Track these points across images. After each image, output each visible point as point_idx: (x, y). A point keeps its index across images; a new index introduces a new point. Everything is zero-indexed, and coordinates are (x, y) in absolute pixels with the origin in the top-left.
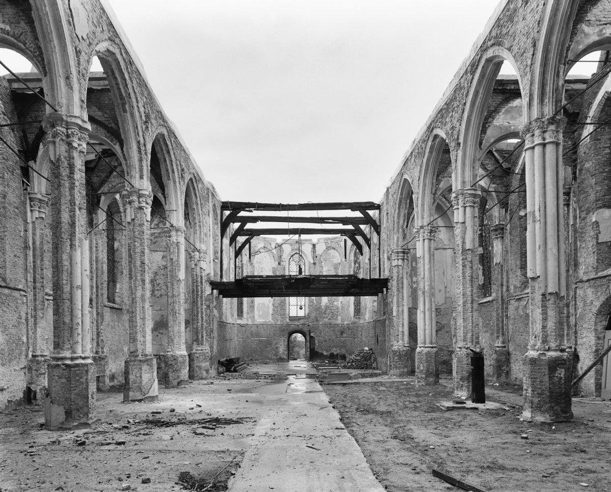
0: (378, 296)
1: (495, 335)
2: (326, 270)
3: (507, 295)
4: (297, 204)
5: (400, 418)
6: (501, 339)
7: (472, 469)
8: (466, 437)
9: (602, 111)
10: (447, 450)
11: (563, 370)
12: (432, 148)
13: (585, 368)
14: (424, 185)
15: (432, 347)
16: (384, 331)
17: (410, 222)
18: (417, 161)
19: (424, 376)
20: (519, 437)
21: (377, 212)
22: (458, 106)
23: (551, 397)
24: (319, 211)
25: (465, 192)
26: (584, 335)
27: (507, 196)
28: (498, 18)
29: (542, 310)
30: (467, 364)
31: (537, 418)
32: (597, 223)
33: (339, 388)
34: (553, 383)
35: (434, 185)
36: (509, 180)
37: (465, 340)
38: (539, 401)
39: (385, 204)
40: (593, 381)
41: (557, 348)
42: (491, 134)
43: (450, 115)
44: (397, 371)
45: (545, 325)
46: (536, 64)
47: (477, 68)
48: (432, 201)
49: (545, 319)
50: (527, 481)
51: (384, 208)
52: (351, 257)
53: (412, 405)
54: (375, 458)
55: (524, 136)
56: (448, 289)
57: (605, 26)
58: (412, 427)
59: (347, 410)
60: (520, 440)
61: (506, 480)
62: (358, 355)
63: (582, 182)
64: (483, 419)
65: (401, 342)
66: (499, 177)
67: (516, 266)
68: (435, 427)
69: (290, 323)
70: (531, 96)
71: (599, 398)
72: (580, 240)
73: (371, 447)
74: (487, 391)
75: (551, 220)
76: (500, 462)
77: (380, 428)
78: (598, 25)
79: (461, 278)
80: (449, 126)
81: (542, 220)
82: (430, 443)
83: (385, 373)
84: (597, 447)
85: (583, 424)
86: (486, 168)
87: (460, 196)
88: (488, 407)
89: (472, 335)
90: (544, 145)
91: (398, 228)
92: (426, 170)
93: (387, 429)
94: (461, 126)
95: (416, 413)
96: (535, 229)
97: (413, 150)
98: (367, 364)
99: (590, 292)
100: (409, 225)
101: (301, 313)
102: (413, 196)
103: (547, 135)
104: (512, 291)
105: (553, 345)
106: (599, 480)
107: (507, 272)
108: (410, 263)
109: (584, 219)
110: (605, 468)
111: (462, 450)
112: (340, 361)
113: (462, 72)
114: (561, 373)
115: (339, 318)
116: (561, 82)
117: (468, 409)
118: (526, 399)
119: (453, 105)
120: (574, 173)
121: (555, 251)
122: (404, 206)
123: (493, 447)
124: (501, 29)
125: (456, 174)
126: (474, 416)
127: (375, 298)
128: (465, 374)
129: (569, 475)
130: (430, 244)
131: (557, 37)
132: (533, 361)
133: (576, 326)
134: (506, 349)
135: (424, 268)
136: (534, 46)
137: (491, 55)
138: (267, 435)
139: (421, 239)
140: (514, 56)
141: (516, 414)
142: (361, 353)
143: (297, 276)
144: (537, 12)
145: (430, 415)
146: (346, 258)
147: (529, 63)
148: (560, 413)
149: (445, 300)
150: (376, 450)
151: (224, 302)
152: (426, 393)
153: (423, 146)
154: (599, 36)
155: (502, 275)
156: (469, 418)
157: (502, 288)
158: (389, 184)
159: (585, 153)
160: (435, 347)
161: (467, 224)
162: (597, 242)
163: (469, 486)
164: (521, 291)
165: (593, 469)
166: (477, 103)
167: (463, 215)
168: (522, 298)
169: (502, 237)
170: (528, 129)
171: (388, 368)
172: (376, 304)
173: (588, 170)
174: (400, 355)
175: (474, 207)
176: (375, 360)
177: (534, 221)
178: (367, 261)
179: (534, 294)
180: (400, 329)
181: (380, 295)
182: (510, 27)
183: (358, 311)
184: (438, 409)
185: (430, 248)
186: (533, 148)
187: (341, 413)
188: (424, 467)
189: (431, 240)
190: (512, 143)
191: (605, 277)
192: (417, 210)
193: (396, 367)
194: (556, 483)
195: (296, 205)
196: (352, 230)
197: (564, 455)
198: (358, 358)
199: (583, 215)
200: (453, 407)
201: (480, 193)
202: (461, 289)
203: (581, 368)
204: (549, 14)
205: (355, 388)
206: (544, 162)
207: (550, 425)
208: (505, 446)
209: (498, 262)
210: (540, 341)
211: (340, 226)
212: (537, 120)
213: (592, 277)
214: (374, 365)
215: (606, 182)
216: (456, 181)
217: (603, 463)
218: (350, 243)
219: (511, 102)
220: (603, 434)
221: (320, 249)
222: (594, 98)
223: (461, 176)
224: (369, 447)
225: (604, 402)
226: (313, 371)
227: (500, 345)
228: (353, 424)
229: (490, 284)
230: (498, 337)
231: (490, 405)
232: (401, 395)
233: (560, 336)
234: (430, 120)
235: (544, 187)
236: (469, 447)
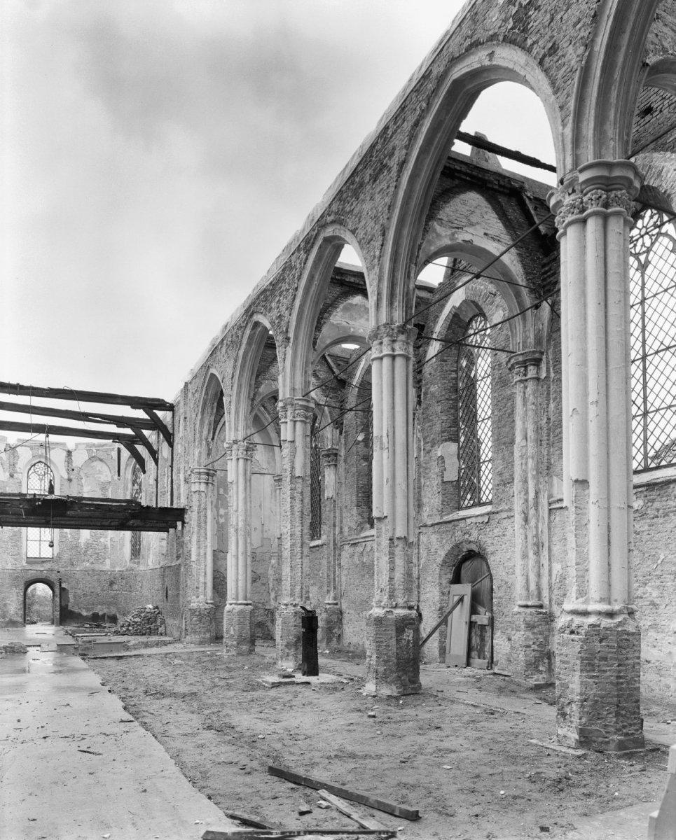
0: (168, 532)
1: (325, 589)
2: (88, 490)
3: (341, 538)
4: (46, 387)
5: (210, 701)
6: (332, 594)
7: (317, 760)
8: (301, 720)
9: (449, 328)
10: (281, 740)
11: (412, 631)
12: (251, 338)
13: (429, 630)
14: (240, 386)
15: (247, 604)
16: (178, 582)
17: (217, 434)
18: (229, 352)
19: (235, 643)
20: (365, 716)
21: (169, 414)
22: (287, 290)
23: (398, 664)
24: (33, 398)
25: (296, 402)
26: (428, 590)
27: (342, 414)
28: (340, 190)
29: (390, 558)
30: (295, 626)
31: (382, 691)
32: (442, 458)
33: (112, 663)
34: (401, 648)
35: (253, 386)
36: (345, 394)
37: (292, 595)
38: (385, 670)
39: (182, 404)
40: (436, 644)
42: (327, 334)
43: (277, 299)
44: (196, 638)
45: (392, 577)
46: (385, 258)
47: (312, 247)
48: (250, 408)
49: (392, 569)
50: (384, 770)
51: (181, 411)
52: (128, 474)
53: (223, 683)
54: (185, 758)
55: (371, 342)
56: (266, 528)
58: (230, 712)
59: (130, 694)
60: (368, 719)
61: (360, 770)
62: (138, 616)
63: (427, 408)
64: (317, 696)
65: (202, 597)
66: (333, 389)
67: (352, 502)
68: (259, 709)
69: (28, 567)
70: (379, 294)
71: (444, 665)
72: (424, 477)
73: (178, 744)
74: (321, 661)
75: (400, 449)
76: (349, 748)
77: (184, 717)
79: (289, 514)
80: (275, 313)
81: (390, 449)
82: (258, 731)
83: (178, 640)
84: (451, 722)
85: (432, 695)
86: (317, 376)
87: (289, 406)
88: (323, 681)
89: (302, 588)
90: (393, 357)
91: (201, 440)
92: (243, 366)
93: (195, 716)
94: (289, 315)
95: (231, 694)
96: (382, 458)
97: (225, 337)
98: (150, 628)
99: (434, 538)
100: (216, 437)
101: (47, 553)
102: (224, 399)
103: (397, 346)
104: (346, 534)
105: (401, 601)
106: (462, 760)
107: (341, 509)
108: (216, 489)
109: (429, 452)
110: (465, 746)
111: (299, 737)
112: (107, 625)
113: (294, 248)
114: (409, 634)
115: (108, 562)
116: (412, 286)
117: (298, 684)
118: (369, 668)
119: (281, 288)
120: (419, 396)
121: (404, 487)
122: (210, 410)
123: (337, 731)
124: (344, 204)
125: (284, 376)
126: (307, 692)
127: (164, 535)
128: (292, 639)
129: (428, 757)
130: (245, 465)
132: (379, 621)
133: (419, 578)
134: (338, 607)
135: (236, 498)
136: (384, 235)
137: (331, 234)
138: (10, 739)
139: (234, 458)
140: (359, 242)
141: (357, 687)
142: (142, 612)
143: (46, 496)
144: (387, 194)
145: (250, 695)
146: (119, 475)
147: (378, 253)
149: (262, 541)
150: (184, 747)
152: (239, 666)
153: (240, 333)
154: (451, 239)
155: (335, 512)
156: (300, 696)
157: (334, 530)
158: (188, 378)
159: (430, 374)
160: (250, 604)
161: (297, 444)
162: (442, 480)
163: (320, 783)
164: (357, 535)
165: (453, 748)
166: (312, 291)
167: (291, 430)
168: (358, 543)
169: (336, 465)
170: (375, 335)
171: (183, 633)
172: (164, 543)
173: (433, 395)
174: (199, 615)
175: (305, 423)
176: (163, 621)
177: (382, 449)
178: (152, 481)
179: (381, 539)
180: (202, 579)
181: (171, 530)
182: (354, 205)
183: (136, 552)
184: (260, 686)
185: (245, 470)
186: (381, 358)
187: (123, 699)
188: (255, 764)
189: (247, 460)
190: (348, 349)
191: (450, 522)
192: (229, 417)
193: (195, 632)
194: (417, 768)
195: (43, 389)
196: (129, 436)
197: (419, 734)
198: (138, 620)
199: (428, 447)
200: (280, 683)
201: (313, 405)
202: (289, 528)
203: (424, 629)
204: (401, 200)
205: (136, 663)
206: (393, 378)
207: (397, 698)
208: (351, 728)
209: (330, 496)
210: (387, 596)
211: (112, 428)
212: (386, 325)
213: (437, 521)
214: (161, 629)
215: (452, 411)
216: (284, 386)
217: (461, 741)
218: (126, 454)
219: (350, 297)
220: (455, 706)
221: (80, 459)
222: (441, 312)
223: (290, 377)
224: (173, 744)
225: (449, 669)
226: (69, 640)
227: (330, 602)
228: (146, 714)
229: (320, 524)
230: (328, 591)
231: (323, 677)
232: (205, 669)
233: (408, 590)
234: (250, 302)
235: (393, 408)
236: (309, 733)
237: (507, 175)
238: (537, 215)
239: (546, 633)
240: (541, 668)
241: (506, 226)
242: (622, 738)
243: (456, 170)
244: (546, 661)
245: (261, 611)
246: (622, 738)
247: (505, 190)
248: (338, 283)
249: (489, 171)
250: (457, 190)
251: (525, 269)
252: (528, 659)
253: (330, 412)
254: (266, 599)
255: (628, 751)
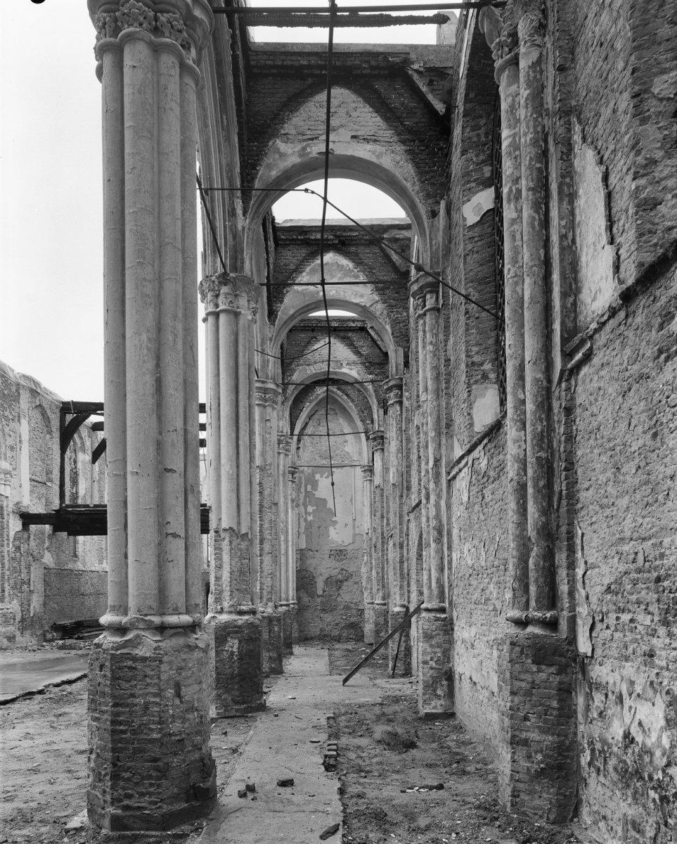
6: (381, 594)
11: (237, 641)
41: (232, 609)
45: (218, 576)
56: (357, 523)
57: (311, 142)
66: (379, 364)
78: (300, 141)
86: (360, 353)
131: (216, 159)
148: (231, 703)
151: (81, 542)
154: (300, 156)
169: (383, 450)
206: (217, 340)
237: (381, 50)
238: (432, 91)
239: (447, 646)
240: (439, 692)
241: (386, 119)
242: (119, 811)
243: (302, 67)
244: (445, 683)
245: (354, 612)
246: (119, 811)
247: (382, 72)
248: (302, 244)
249: (352, 53)
250: (310, 91)
251: (418, 168)
252: (426, 679)
253: (375, 391)
254: (359, 598)
255: (128, 833)
